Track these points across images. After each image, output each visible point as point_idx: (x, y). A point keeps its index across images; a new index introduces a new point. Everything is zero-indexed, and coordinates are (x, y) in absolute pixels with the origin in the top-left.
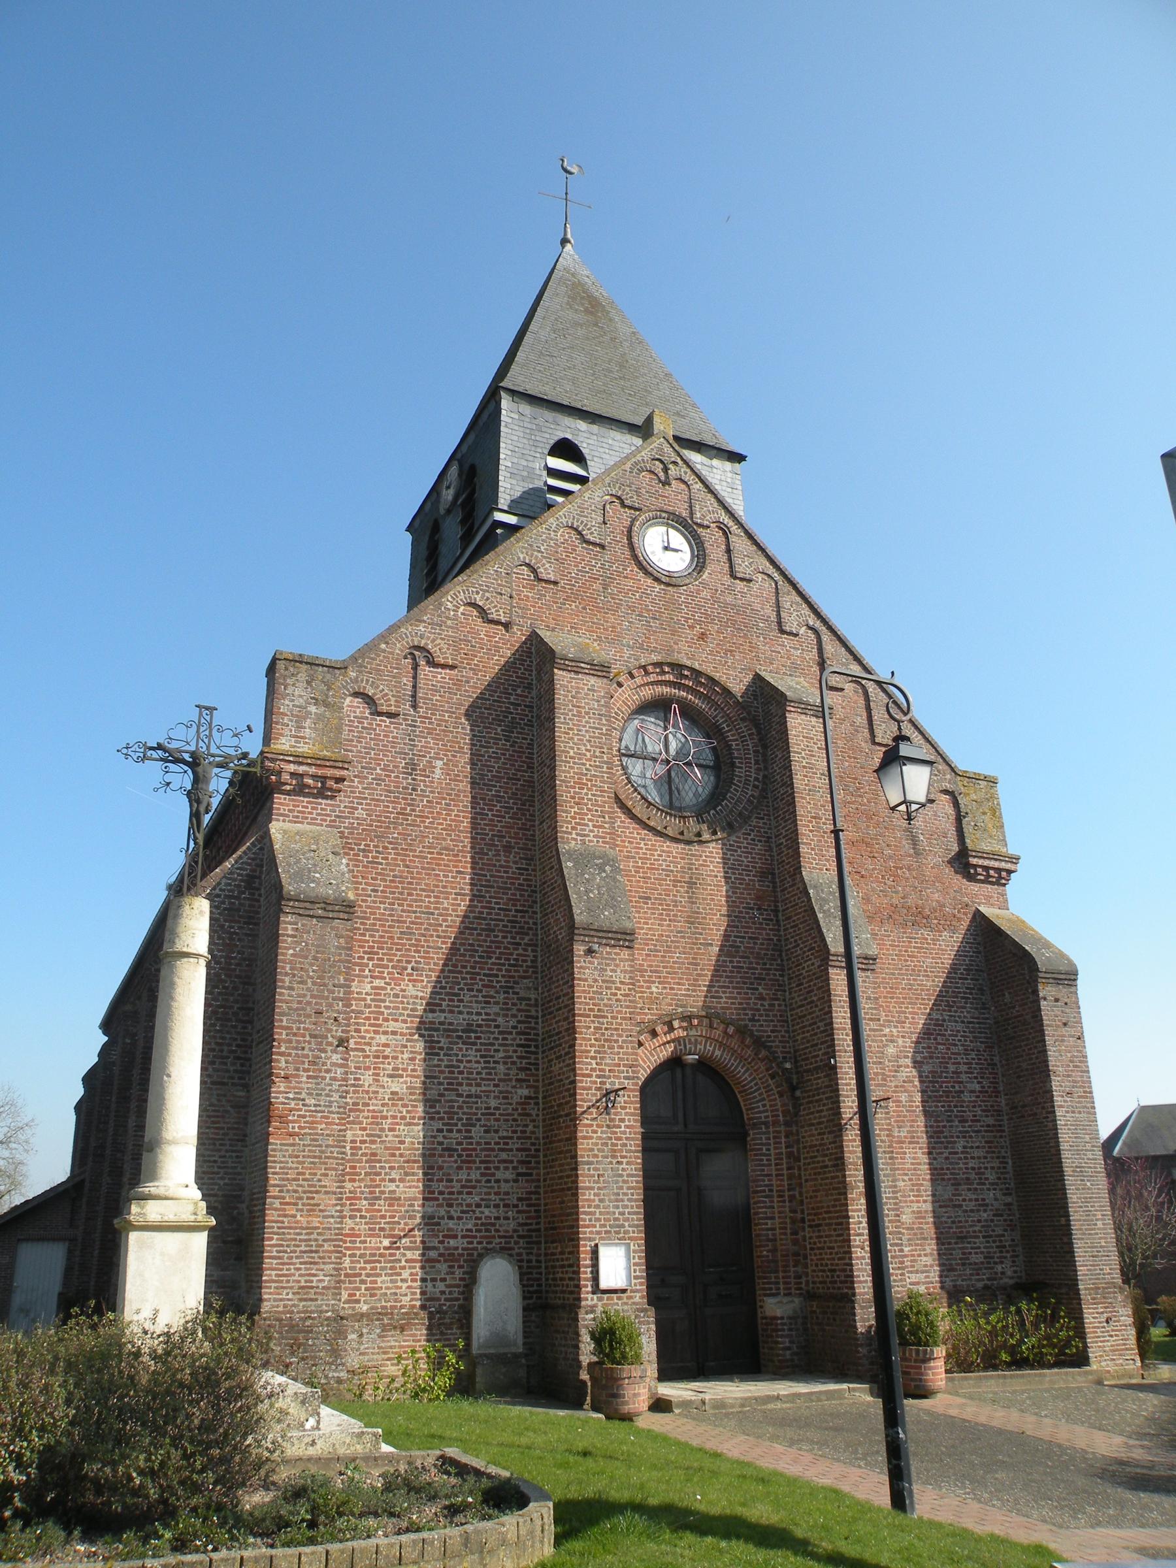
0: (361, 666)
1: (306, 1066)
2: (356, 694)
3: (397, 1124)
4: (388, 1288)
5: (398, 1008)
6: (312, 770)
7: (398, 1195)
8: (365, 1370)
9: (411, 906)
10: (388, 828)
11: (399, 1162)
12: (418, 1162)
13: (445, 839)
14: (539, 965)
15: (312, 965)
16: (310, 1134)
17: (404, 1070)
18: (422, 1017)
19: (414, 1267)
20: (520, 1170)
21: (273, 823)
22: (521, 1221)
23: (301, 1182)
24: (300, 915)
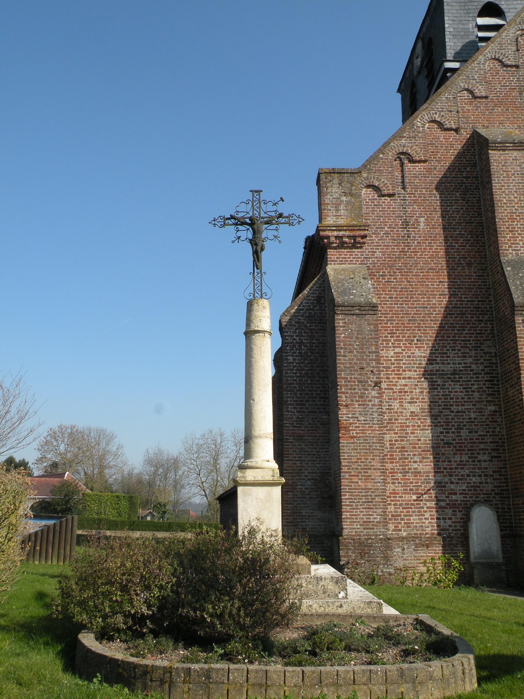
0: (369, 170)
1: (357, 399)
2: (368, 186)
3: (416, 430)
4: (417, 523)
5: (411, 364)
6: (347, 233)
7: (419, 470)
8: (406, 569)
9: (413, 304)
10: (395, 261)
11: (418, 451)
12: (430, 451)
13: (430, 264)
14: (495, 332)
15: (355, 342)
16: (363, 437)
17: (417, 399)
18: (425, 368)
19: (432, 511)
20: (493, 455)
21: (329, 266)
22: (496, 484)
23: (360, 464)
24: (346, 314)
